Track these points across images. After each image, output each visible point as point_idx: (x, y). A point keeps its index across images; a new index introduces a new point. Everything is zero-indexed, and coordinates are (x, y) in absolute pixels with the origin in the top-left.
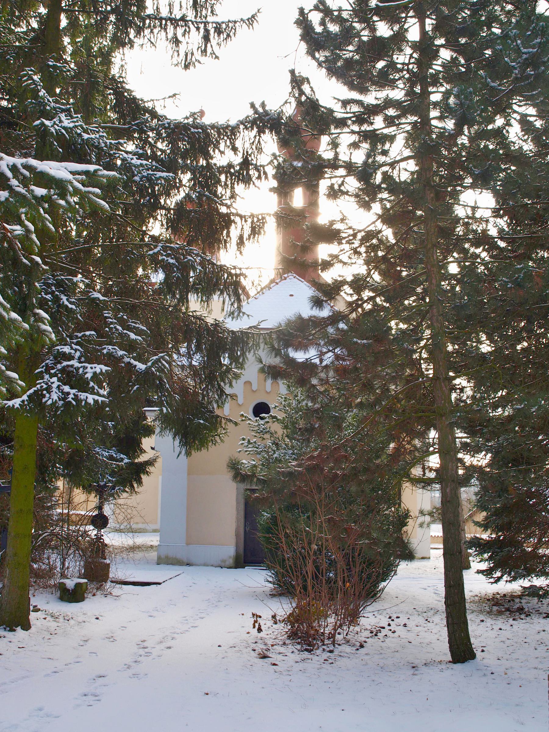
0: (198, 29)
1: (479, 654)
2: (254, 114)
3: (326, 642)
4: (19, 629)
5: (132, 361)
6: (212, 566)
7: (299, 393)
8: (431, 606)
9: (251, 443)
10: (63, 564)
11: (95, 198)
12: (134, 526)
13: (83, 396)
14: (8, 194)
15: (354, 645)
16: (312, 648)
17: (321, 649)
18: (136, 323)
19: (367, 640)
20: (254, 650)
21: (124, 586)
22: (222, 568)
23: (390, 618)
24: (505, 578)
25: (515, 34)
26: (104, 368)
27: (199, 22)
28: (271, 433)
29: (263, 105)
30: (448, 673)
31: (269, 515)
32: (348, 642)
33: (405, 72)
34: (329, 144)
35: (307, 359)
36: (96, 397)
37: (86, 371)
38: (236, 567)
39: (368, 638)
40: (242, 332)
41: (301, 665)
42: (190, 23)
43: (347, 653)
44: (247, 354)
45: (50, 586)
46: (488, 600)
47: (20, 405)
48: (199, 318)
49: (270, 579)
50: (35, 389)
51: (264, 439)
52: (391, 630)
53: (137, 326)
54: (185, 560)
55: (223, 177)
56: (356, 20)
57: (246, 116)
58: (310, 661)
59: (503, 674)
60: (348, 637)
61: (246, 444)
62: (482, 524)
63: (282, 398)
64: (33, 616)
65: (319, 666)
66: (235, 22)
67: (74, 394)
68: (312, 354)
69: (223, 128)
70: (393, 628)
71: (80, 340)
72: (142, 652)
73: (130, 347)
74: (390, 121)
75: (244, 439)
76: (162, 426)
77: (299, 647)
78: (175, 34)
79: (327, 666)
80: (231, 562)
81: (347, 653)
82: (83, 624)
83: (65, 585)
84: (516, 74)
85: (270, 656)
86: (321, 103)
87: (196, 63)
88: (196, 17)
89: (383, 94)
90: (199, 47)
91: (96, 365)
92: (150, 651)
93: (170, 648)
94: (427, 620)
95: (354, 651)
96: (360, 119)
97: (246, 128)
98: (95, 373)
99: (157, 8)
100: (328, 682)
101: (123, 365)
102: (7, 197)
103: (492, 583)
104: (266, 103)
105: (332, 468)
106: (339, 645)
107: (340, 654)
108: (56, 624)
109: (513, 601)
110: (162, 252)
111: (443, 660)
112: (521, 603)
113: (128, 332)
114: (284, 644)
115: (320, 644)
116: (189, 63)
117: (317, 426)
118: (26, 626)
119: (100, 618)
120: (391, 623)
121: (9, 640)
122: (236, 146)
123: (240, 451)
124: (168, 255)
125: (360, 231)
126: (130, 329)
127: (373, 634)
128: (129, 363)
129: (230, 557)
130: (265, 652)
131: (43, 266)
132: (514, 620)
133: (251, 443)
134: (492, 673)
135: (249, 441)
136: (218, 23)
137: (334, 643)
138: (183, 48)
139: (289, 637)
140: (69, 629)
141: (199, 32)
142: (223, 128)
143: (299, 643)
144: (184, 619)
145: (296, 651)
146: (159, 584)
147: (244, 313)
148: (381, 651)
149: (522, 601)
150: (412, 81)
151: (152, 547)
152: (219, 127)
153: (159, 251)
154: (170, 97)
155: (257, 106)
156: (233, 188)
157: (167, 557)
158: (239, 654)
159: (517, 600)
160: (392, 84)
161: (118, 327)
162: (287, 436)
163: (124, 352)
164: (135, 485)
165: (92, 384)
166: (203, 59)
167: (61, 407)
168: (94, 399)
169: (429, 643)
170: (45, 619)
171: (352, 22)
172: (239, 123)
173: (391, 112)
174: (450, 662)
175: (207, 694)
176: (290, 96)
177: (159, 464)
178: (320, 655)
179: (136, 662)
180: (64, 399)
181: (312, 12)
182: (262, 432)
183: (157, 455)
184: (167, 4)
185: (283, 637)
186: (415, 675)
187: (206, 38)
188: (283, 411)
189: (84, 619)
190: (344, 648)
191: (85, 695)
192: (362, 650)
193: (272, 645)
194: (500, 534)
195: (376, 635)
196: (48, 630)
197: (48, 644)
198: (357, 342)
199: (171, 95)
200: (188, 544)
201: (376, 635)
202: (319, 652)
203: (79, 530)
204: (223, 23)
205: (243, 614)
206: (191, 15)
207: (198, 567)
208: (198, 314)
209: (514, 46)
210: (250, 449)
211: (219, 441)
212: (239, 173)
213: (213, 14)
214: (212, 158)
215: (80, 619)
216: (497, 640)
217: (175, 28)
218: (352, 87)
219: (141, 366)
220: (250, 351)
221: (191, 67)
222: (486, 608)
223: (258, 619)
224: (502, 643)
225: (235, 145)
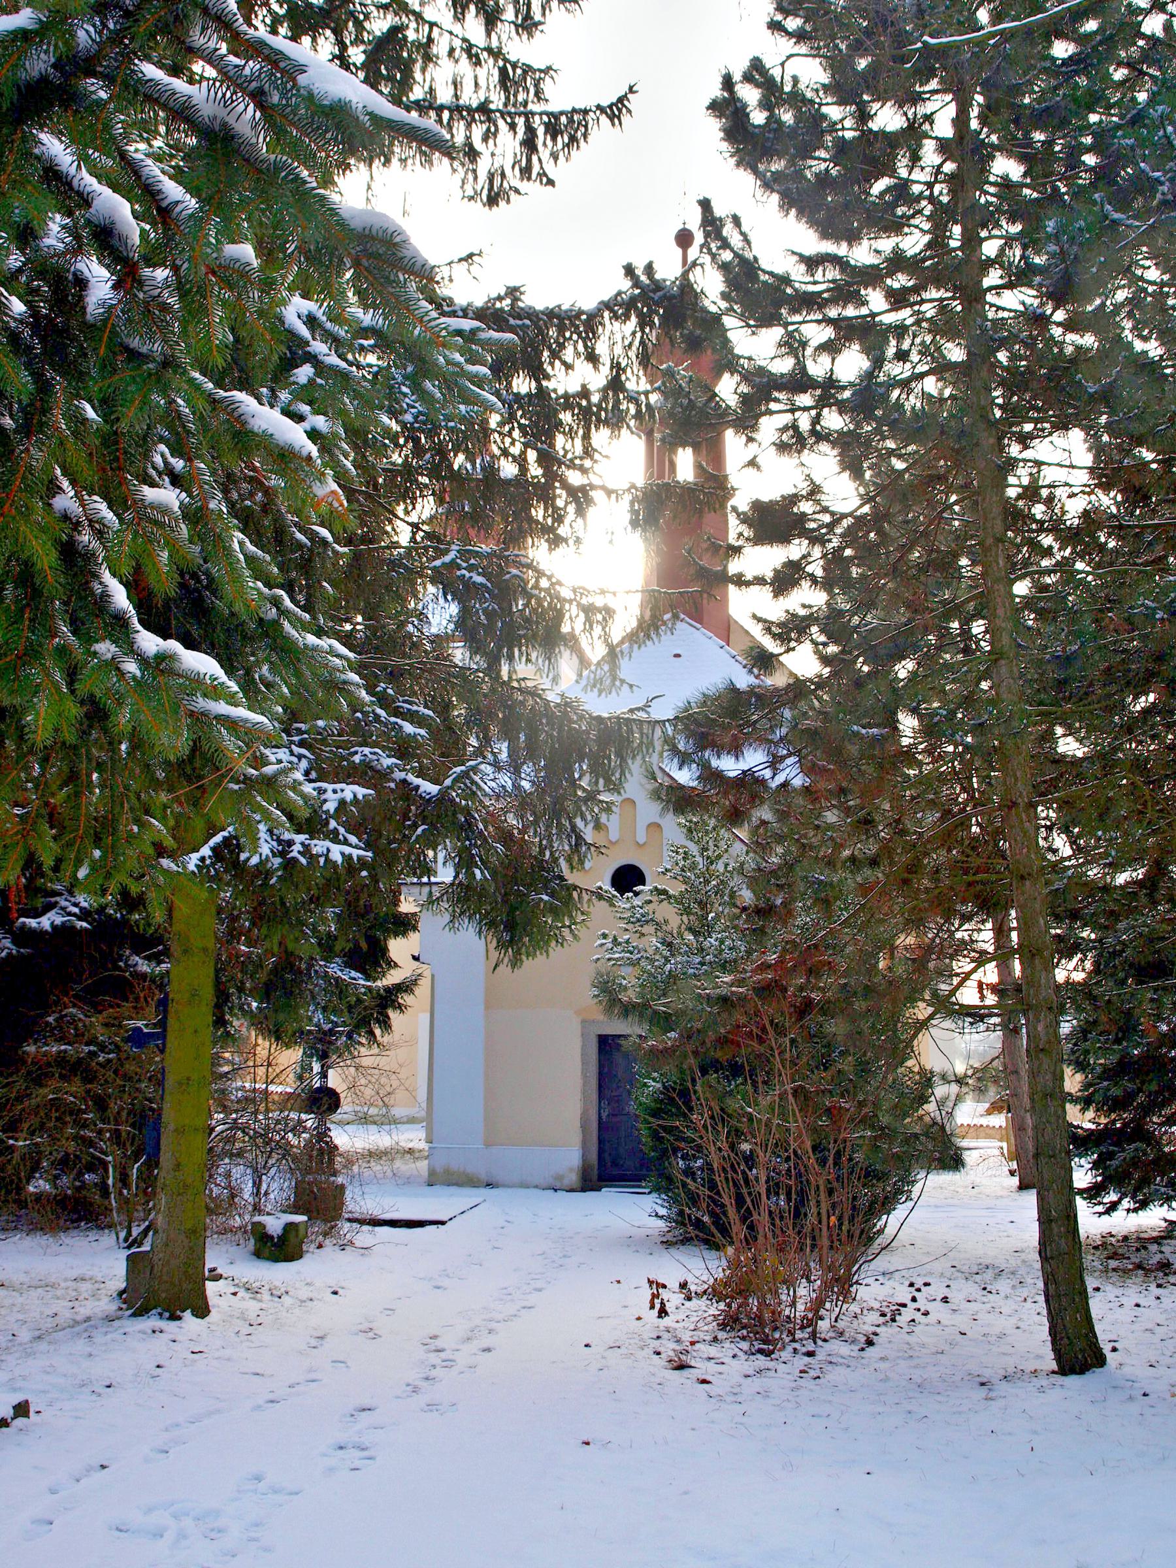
0: (513, 127)
1: (1110, 1356)
2: (632, 287)
3: (799, 1335)
4: (187, 1314)
5: (411, 778)
6: (536, 1187)
7: (711, 843)
8: (988, 1261)
9: (620, 944)
10: (257, 1185)
11: (472, 387)
12: (397, 1112)
13: (319, 846)
14: (313, 370)
15: (854, 1341)
16: (771, 1347)
17: (789, 1349)
18: (410, 703)
19: (878, 1330)
20: (659, 1353)
21: (377, 1229)
22: (556, 1190)
23: (911, 1285)
24: (1126, 1203)
25: (1162, 113)
26: (361, 791)
27: (515, 114)
28: (657, 924)
29: (649, 269)
30: (1054, 1395)
31: (659, 1085)
32: (841, 1334)
33: (924, 203)
34: (780, 346)
35: (744, 772)
36: (347, 850)
37: (323, 797)
38: (583, 1190)
39: (878, 1326)
40: (618, 718)
41: (757, 1383)
42: (498, 115)
43: (843, 1357)
44: (630, 762)
45: (233, 1231)
46: (1096, 1248)
47: (197, 866)
48: (534, 693)
49: (663, 1212)
50: (225, 834)
51: (643, 935)
52: (919, 1310)
53: (415, 708)
54: (484, 1177)
55: (566, 417)
56: (829, 100)
57: (615, 292)
58: (772, 1373)
59: (1168, 1396)
60: (841, 1325)
61: (610, 946)
62: (1078, 1098)
63: (677, 853)
64: (212, 1288)
65: (794, 1385)
66: (586, 112)
67: (302, 844)
68: (754, 759)
69: (569, 319)
70: (922, 1304)
71: (306, 736)
72: (434, 1358)
73: (404, 749)
74: (898, 299)
75: (605, 936)
76: (454, 911)
77: (745, 1345)
78: (468, 138)
79: (807, 1382)
80: (573, 1178)
81: (843, 1357)
82: (309, 1303)
83: (264, 1227)
84: (1163, 194)
85: (693, 1363)
86: (764, 264)
87: (512, 194)
88: (506, 105)
89: (886, 244)
90: (515, 163)
91: (343, 786)
92: (451, 1357)
93: (488, 1350)
94: (985, 1289)
95: (856, 1353)
96: (845, 293)
97: (615, 317)
98: (342, 803)
99: (431, 88)
100: (820, 1416)
101: (392, 785)
102: (311, 375)
103: (1100, 1214)
104: (654, 266)
105: (801, 989)
106: (825, 1340)
107: (829, 1359)
108: (259, 1305)
109: (1145, 1248)
110: (459, 561)
111: (1038, 1368)
112: (1161, 1252)
113: (399, 721)
114: (715, 1339)
115: (787, 1340)
116: (498, 195)
117: (779, 902)
118: (202, 1311)
119: (341, 1291)
120: (917, 1294)
121: (173, 1337)
122: (597, 352)
123: (598, 959)
124: (470, 568)
125: (844, 516)
126: (397, 712)
127: (888, 1318)
128: (404, 781)
129: (571, 1170)
130: (683, 1357)
131: (337, 547)
132: (1159, 1286)
133: (620, 944)
134: (1145, 1395)
135: (615, 939)
136: (552, 114)
137: (814, 1336)
138: (484, 166)
139: (723, 1326)
140: (284, 1314)
141: (515, 133)
142: (569, 319)
143: (743, 1338)
144: (505, 1291)
145: (740, 1353)
146: (443, 1223)
147: (623, 681)
148: (911, 1353)
149: (1163, 1249)
150: (941, 218)
151: (410, 1151)
152: (563, 315)
153: (453, 559)
154: (460, 260)
155: (639, 272)
156: (587, 437)
157: (447, 1171)
158: (630, 1361)
159: (1153, 1248)
160: (897, 227)
161: (380, 711)
162: (690, 929)
163: (394, 760)
164: (378, 1032)
165: (333, 824)
166: (524, 186)
167: (277, 869)
168: (343, 854)
169: (1002, 1336)
170: (235, 1294)
171: (820, 105)
172: (602, 307)
173: (901, 281)
174: (1053, 1372)
175: (588, 1443)
176: (701, 252)
177: (423, 989)
178: (788, 1363)
179: (427, 1379)
180: (282, 854)
181: (792, 59)
182: (639, 921)
183: (419, 971)
184: (450, 81)
185: (710, 1327)
186: (991, 1399)
187: (529, 143)
188: (680, 878)
189: (311, 1295)
190: (835, 1347)
191: (341, 1448)
192: (870, 1350)
193: (693, 1343)
194: (1113, 1116)
195: (893, 1320)
196: (243, 1317)
197: (248, 1344)
198: (858, 733)
199: (464, 255)
200: (488, 1144)
201: (893, 1320)
202: (786, 1354)
203: (286, 1118)
204: (562, 113)
205: (619, 1282)
206: (497, 101)
207: (509, 1190)
208: (530, 684)
209: (1160, 139)
210: (617, 955)
211: (569, 937)
212: (600, 408)
213: (539, 99)
214: (548, 377)
215: (304, 1293)
216: (1135, 1327)
217: (469, 126)
218: (826, 232)
219: (429, 788)
220: (634, 757)
221: (502, 204)
222: (1095, 1263)
223: (660, 1290)
224: (1148, 1334)
225: (593, 349)
